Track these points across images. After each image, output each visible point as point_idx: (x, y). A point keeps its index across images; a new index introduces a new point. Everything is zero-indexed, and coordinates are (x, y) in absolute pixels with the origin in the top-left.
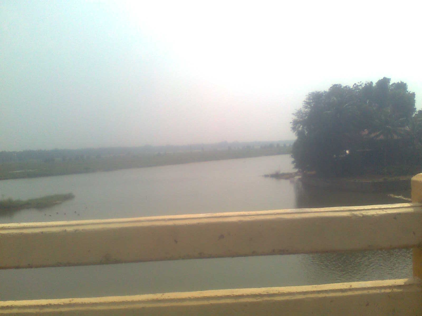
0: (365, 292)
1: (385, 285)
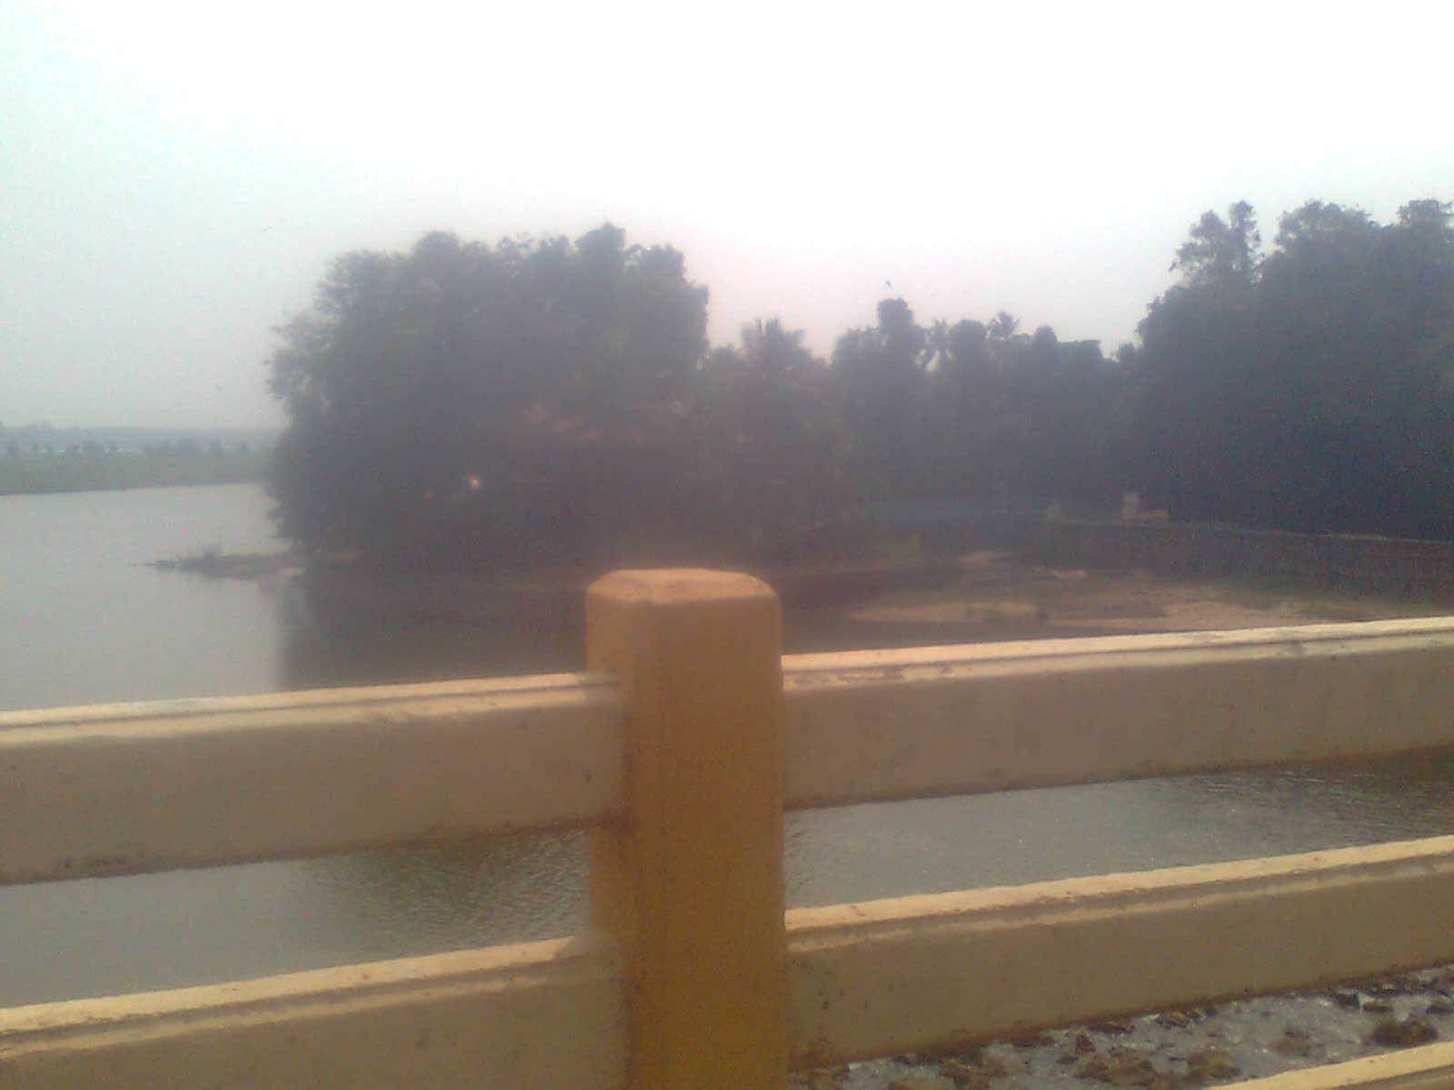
0: (416, 996)
1: (489, 965)
